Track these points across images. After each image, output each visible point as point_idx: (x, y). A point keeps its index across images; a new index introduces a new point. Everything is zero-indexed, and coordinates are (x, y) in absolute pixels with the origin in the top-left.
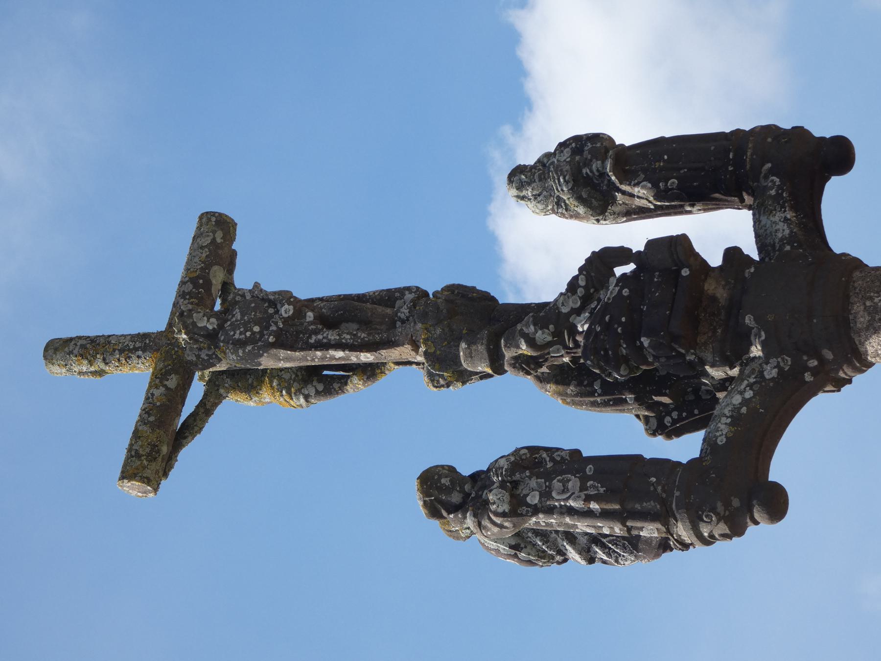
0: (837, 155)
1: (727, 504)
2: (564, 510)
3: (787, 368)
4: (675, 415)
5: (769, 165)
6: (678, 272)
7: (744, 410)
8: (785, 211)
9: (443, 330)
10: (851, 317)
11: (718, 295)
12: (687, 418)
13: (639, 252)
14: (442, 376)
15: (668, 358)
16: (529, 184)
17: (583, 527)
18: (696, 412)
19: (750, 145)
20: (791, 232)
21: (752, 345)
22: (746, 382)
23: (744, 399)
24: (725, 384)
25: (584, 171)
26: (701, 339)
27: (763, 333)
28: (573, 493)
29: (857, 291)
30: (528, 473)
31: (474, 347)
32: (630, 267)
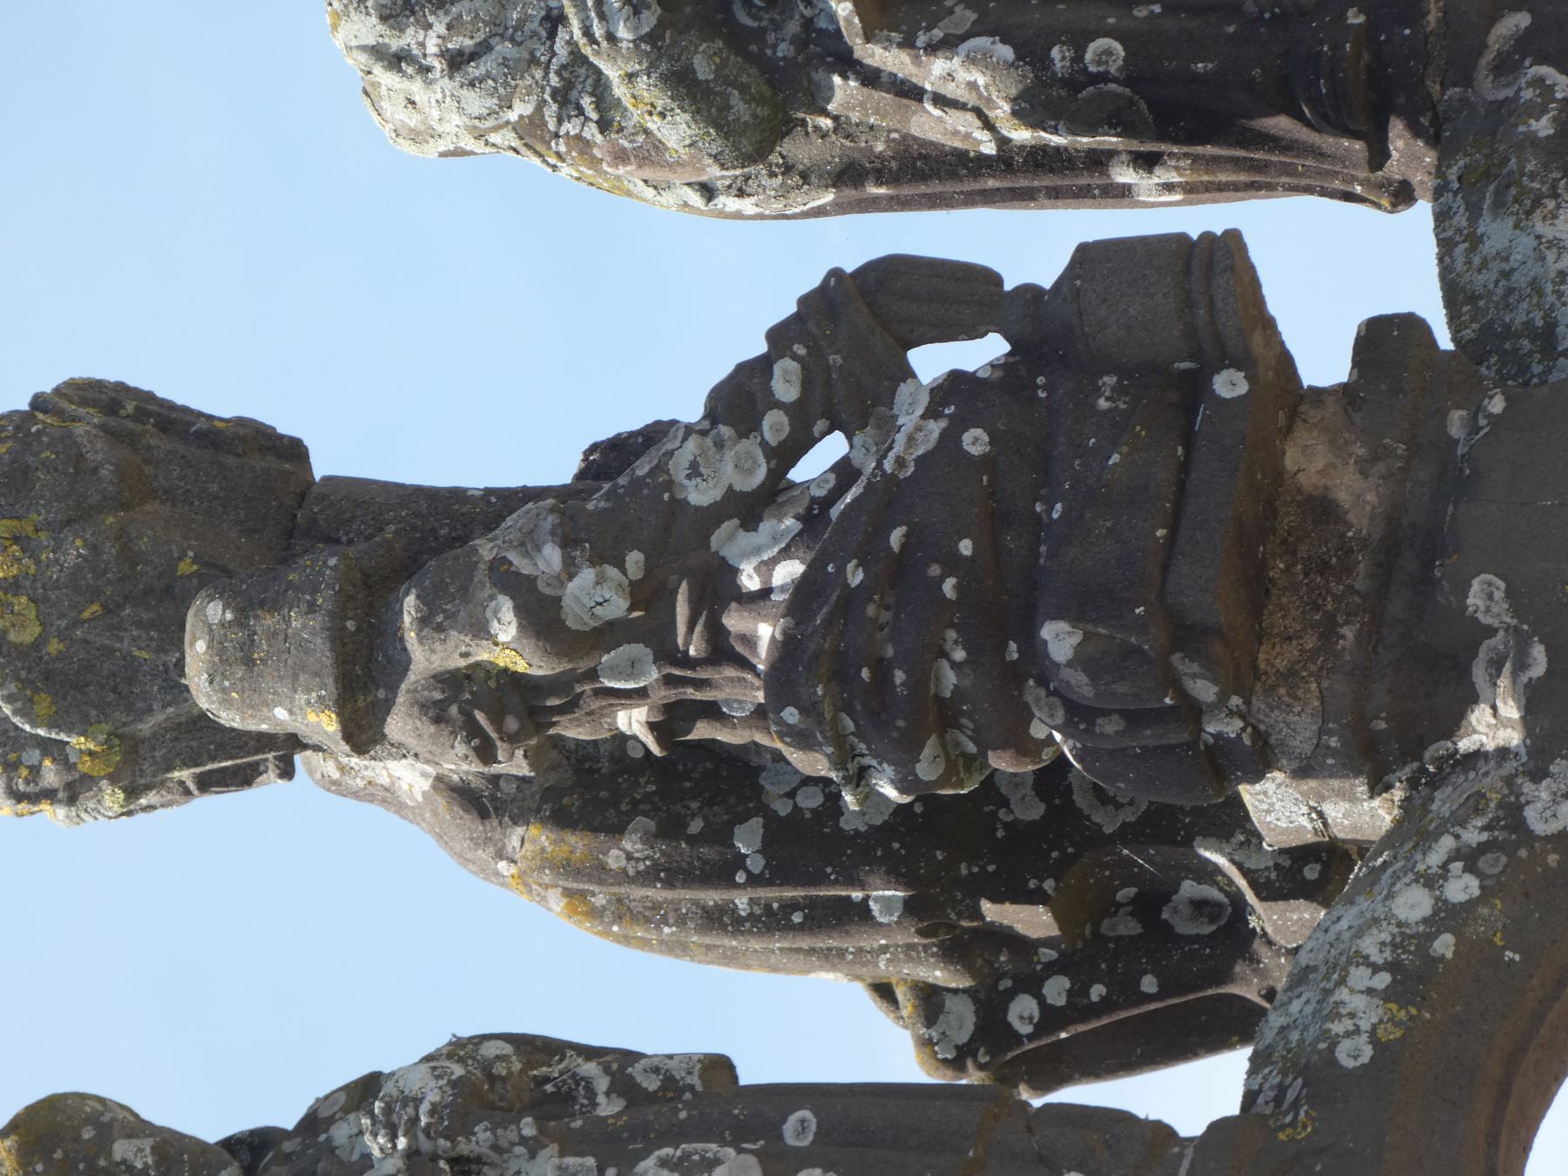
4: (1057, 990)
7: (1445, 945)
9: (94, 549)
11: (1342, 496)
12: (1106, 1006)
13: (1030, 293)
15: (1134, 719)
18: (1149, 984)
21: (1473, 699)
22: (1446, 843)
23: (1442, 905)
24: (1317, 869)
26: (1275, 658)
27: (1539, 653)
31: (269, 621)
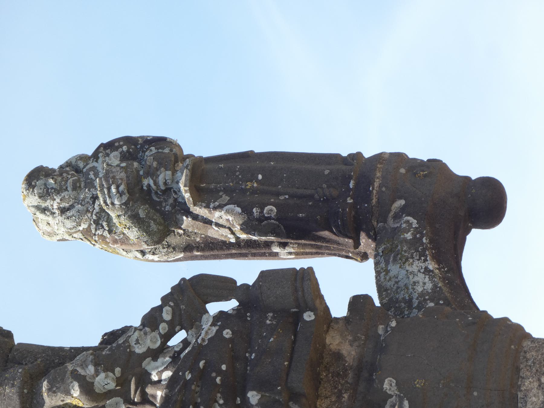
0: (485, 203)
5: (402, 202)
6: (298, 317)
8: (425, 260)
10: (520, 395)
11: (344, 352)
13: (245, 286)
16: (58, 192)
19: (378, 174)
20: (435, 286)
25: (145, 182)
29: (530, 363)
32: (230, 305)
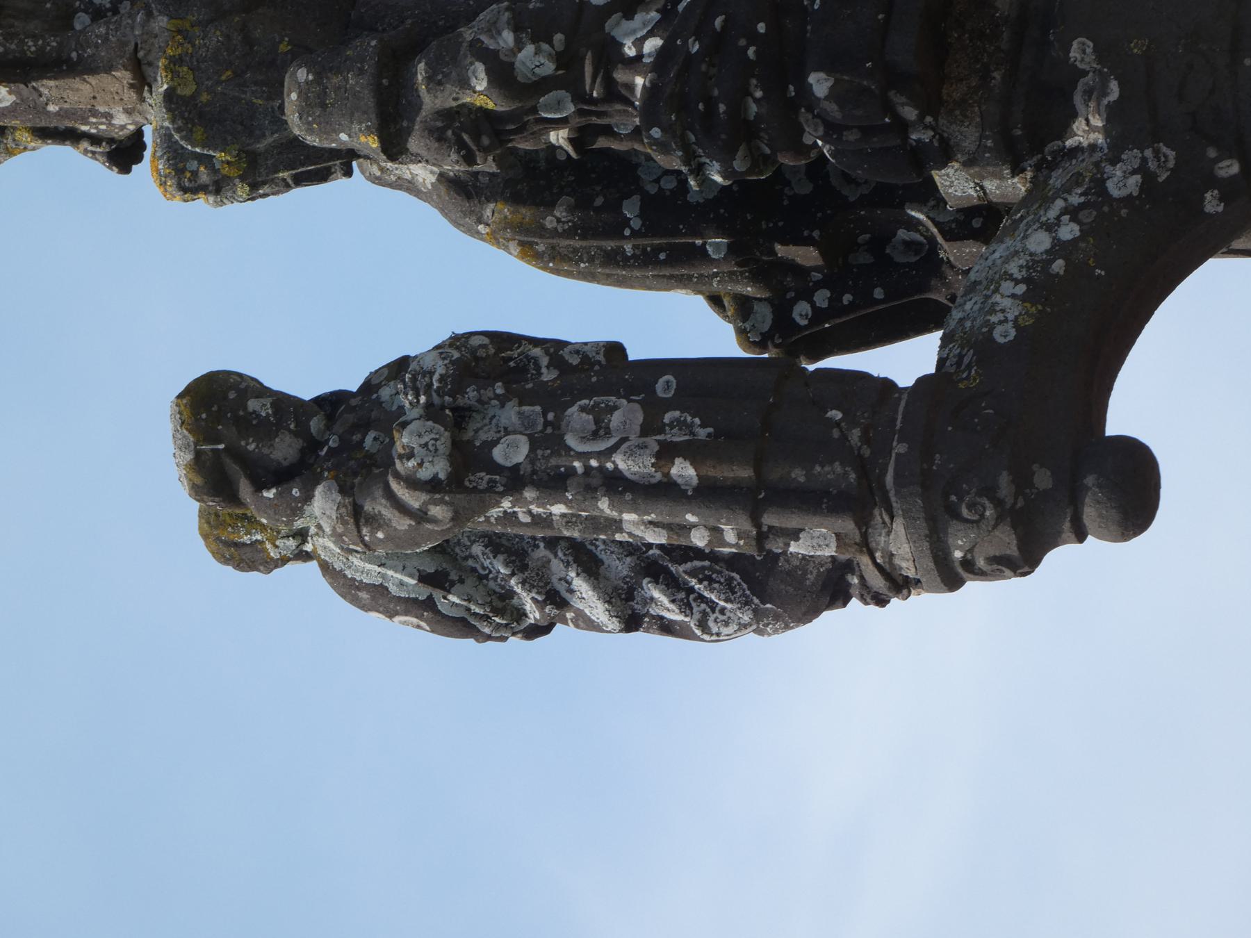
1: (1022, 481)
2: (596, 481)
3: (1163, 177)
4: (822, 298)
7: (1058, 266)
9: (228, 37)
14: (206, 160)
17: (639, 526)
18: (878, 293)
22: (1059, 204)
23: (1057, 242)
24: (983, 221)
27: (1114, 86)
28: (624, 440)
30: (499, 389)
31: (336, 80)
